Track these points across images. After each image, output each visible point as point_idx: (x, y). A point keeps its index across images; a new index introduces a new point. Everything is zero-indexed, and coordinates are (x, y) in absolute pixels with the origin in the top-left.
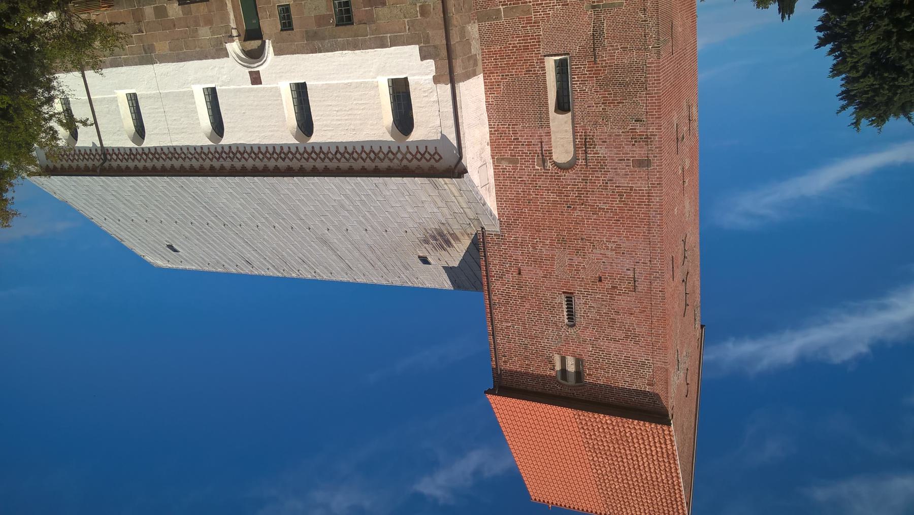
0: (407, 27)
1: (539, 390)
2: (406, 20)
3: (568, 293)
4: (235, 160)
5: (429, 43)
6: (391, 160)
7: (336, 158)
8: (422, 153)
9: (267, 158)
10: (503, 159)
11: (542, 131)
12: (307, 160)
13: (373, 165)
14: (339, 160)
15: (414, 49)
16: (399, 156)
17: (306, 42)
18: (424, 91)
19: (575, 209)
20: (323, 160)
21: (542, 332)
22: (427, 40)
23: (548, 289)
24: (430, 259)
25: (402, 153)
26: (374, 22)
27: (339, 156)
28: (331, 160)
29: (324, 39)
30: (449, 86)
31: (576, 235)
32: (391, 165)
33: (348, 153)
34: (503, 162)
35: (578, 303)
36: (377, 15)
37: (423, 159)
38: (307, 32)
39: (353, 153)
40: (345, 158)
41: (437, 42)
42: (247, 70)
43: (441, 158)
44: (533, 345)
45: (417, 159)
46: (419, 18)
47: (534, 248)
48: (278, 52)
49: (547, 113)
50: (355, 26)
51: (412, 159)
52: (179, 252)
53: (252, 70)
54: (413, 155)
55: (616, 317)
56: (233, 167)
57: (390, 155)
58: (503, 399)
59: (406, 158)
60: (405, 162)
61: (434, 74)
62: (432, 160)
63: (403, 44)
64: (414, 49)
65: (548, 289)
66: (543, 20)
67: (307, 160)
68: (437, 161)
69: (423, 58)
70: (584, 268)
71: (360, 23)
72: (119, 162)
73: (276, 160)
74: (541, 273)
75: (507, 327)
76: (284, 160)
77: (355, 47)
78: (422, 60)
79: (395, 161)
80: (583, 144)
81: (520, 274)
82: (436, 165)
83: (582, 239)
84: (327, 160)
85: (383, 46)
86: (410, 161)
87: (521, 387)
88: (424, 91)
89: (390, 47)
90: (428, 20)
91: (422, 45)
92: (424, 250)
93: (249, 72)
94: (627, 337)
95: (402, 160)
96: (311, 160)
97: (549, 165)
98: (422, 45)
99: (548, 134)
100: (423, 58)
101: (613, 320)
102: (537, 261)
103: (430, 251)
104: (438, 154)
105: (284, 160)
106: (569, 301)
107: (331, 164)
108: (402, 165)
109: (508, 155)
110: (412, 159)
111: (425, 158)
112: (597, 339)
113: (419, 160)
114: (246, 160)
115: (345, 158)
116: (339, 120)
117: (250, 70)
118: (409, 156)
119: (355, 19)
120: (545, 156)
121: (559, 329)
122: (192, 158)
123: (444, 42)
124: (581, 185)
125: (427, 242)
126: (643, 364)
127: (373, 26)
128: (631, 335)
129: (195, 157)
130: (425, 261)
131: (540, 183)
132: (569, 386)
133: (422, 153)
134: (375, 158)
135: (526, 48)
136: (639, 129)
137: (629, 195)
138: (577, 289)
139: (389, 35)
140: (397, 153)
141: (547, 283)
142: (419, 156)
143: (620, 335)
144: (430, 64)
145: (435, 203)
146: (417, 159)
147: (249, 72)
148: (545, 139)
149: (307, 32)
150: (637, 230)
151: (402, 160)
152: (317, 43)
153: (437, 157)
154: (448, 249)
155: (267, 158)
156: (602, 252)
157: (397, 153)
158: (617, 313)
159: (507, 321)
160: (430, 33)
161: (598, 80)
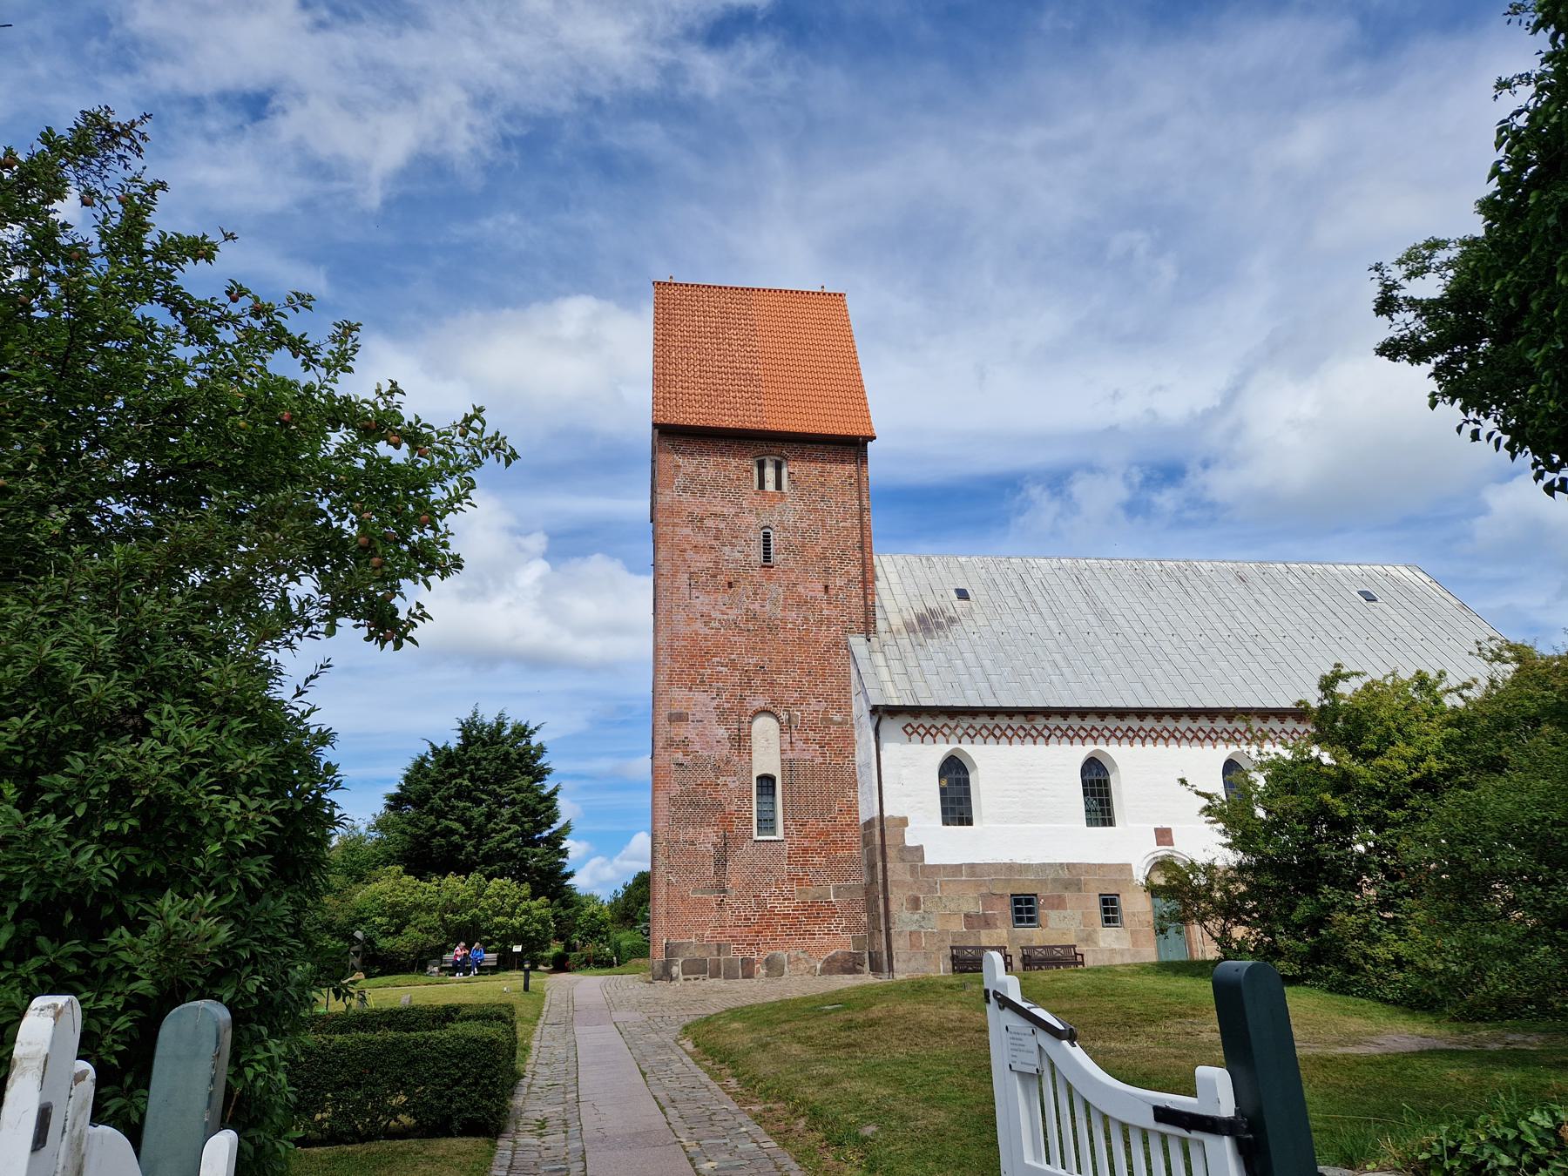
0: (938, 886)
1: (809, 446)
2: (939, 894)
3: (768, 567)
4: (1207, 730)
5: (911, 866)
6: (971, 726)
7: (1050, 730)
8: (928, 735)
9: (1156, 731)
10: (840, 724)
11: (790, 755)
12: (1094, 728)
13: (997, 720)
14: (1046, 727)
15: (930, 859)
16: (959, 732)
17: (1082, 878)
18: (920, 808)
19: (756, 665)
20: (1070, 728)
21: (801, 518)
22: (913, 870)
23: (792, 570)
24: (954, 596)
25: (956, 735)
26: (982, 896)
27: (1046, 733)
28: (1058, 728)
29: (1055, 880)
30: (886, 814)
31: (756, 635)
32: (971, 721)
33: (1032, 737)
34: (840, 720)
35: (757, 556)
36: (977, 903)
37: (927, 727)
38: (1079, 890)
39: (1062, 737)
40: (1037, 730)
41: (900, 865)
42: (1177, 847)
43: (904, 729)
44: (814, 502)
45: (936, 728)
46: (921, 896)
47: (806, 618)
48: (1125, 868)
49: (783, 776)
50: (1009, 892)
51: (942, 727)
52: (1361, 593)
53: (1167, 847)
54: (1222, 738)
55: (713, 542)
56: (1212, 720)
57: (972, 732)
58: (851, 432)
59: (950, 728)
60: (952, 724)
61: (906, 829)
62: (991, 728)
63: (945, 867)
64: (930, 859)
65: (792, 570)
66: (783, 881)
67: (1094, 728)
68: (910, 725)
69: (920, 849)
70: (748, 597)
71: (1001, 896)
72: (1194, 727)
73: (1141, 729)
74: (800, 589)
75: (845, 520)
76: (1130, 729)
77: (1010, 867)
78: (922, 846)
79: (965, 726)
80: (741, 741)
81: (826, 587)
82: (910, 720)
83: (748, 630)
84: (1064, 728)
85: (972, 866)
86: (945, 725)
87: (832, 447)
88: (920, 808)
89: (961, 865)
90: (910, 893)
91: (920, 864)
92: (958, 610)
93: (1173, 845)
94: (702, 520)
95: (957, 726)
96: (1088, 728)
97: (784, 717)
98: (920, 864)
99: (783, 752)
100: (920, 849)
101: (717, 538)
102: (802, 603)
103: (950, 606)
104: (907, 733)
105: (1130, 729)
106: (767, 557)
107: (1058, 723)
108: (956, 721)
109: (833, 728)
110: (942, 727)
111: (925, 728)
112: (736, 515)
113: (934, 726)
114: (1189, 729)
115: (1037, 730)
116: (1042, 778)
117: (1171, 848)
118: (946, 731)
119: (1008, 900)
120: (786, 727)
121: (781, 522)
122: (1055, 729)
123: (889, 866)
124: (747, 692)
125: (952, 620)
126: (684, 490)
127: (984, 890)
128: (697, 521)
129: (1275, 733)
130: (962, 594)
131: (796, 695)
132: (773, 455)
133: (928, 735)
134: (994, 729)
135: (805, 851)
136: (679, 756)
137: (693, 682)
138: (758, 573)
139: (964, 878)
140: (963, 735)
141: (793, 576)
142: (933, 731)
143: (709, 523)
144: (910, 841)
145: (922, 673)
146: (936, 728)
147: (1173, 845)
148: (787, 746)
149: (1079, 890)
150: (685, 643)
151: (957, 726)
152: (1065, 875)
153: (909, 730)
154: (925, 612)
155: (1156, 731)
156: (726, 617)
157: (963, 735)
158: (712, 547)
159: (845, 528)
160: (908, 878)
161: (723, 810)
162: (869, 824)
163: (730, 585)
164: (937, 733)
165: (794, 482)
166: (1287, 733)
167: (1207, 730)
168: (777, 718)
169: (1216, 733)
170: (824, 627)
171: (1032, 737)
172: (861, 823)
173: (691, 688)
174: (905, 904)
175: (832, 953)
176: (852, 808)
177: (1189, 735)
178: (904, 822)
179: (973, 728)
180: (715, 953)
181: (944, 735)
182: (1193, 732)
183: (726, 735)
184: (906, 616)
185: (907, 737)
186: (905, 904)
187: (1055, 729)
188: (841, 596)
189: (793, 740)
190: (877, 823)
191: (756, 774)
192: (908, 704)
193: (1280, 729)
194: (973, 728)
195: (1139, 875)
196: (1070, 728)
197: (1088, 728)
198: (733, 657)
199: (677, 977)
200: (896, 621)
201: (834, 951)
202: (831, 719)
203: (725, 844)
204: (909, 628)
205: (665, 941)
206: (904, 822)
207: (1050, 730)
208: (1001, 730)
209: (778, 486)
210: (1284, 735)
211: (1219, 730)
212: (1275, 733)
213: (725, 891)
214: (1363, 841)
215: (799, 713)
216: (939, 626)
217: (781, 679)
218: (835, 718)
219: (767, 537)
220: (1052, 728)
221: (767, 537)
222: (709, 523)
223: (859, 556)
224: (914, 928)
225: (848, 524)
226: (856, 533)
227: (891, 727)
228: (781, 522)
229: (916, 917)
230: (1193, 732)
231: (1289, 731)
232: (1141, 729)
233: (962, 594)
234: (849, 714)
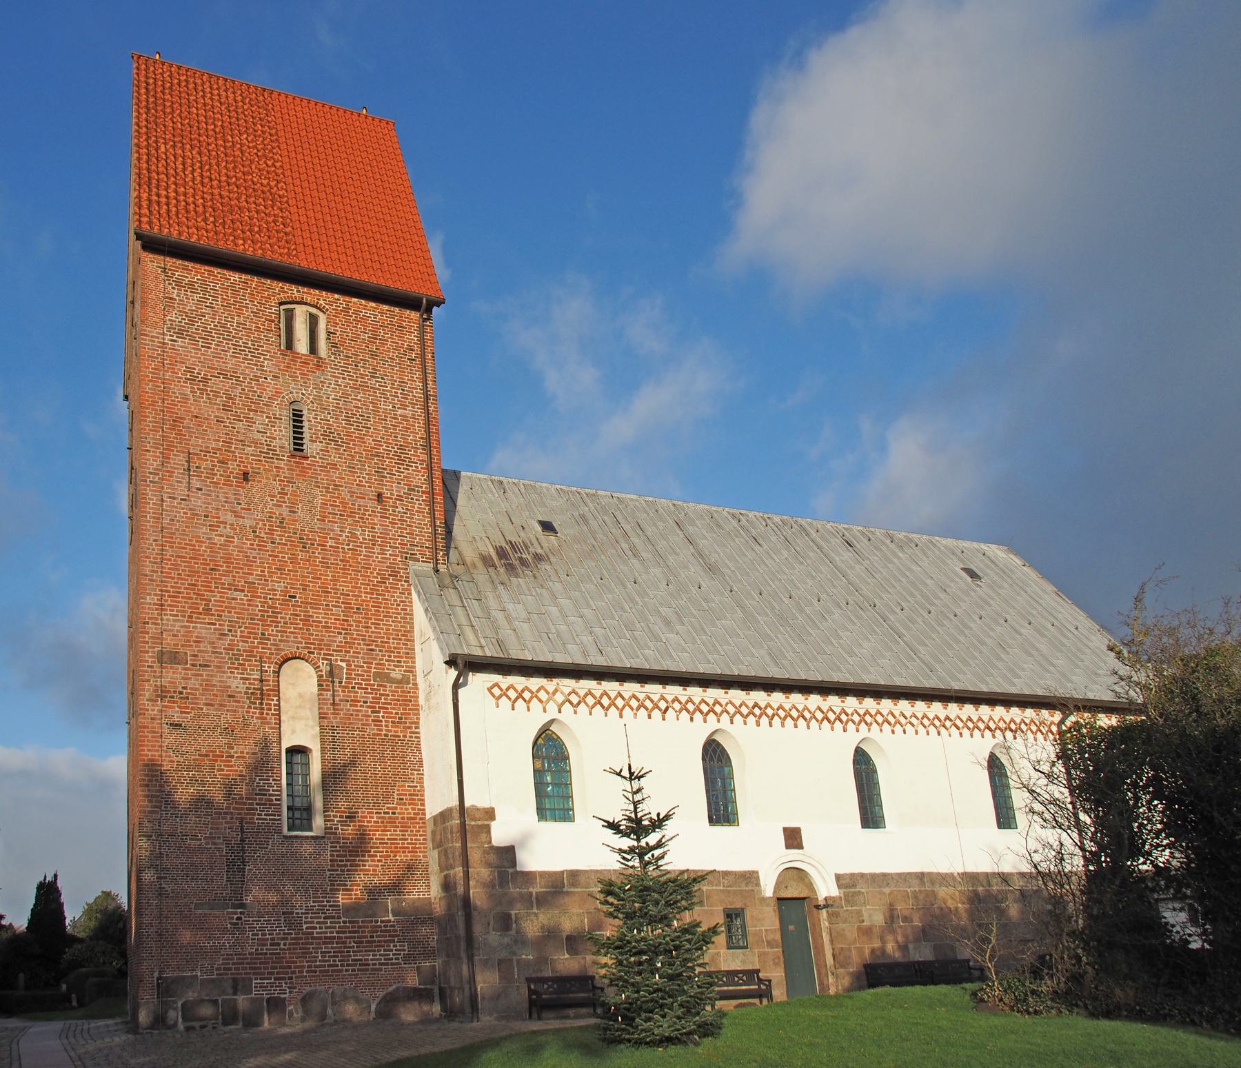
4: (838, 710)
7: (667, 701)
10: (399, 682)
12: (716, 702)
23: (334, 467)
24: (539, 528)
27: (663, 705)
30: (467, 804)
33: (646, 708)
35: (283, 435)
37: (504, 688)
40: (652, 701)
43: (489, 690)
45: (530, 691)
47: (354, 536)
48: (750, 878)
49: (323, 749)
52: (962, 569)
57: (575, 699)
73: (768, 705)
75: (404, 407)
89: (563, 872)
92: (545, 545)
95: (556, 691)
96: (711, 702)
97: (325, 668)
98: (511, 870)
99: (322, 717)
101: (227, 408)
104: (493, 696)
112: (256, 379)
114: (819, 708)
115: (652, 701)
121: (318, 399)
125: (538, 558)
126: (180, 334)
129: (906, 718)
130: (547, 527)
131: (340, 638)
134: (601, 696)
136: (175, 713)
137: (194, 608)
142: (527, 695)
143: (216, 384)
145: (508, 618)
151: (556, 691)
153: (496, 691)
154: (504, 545)
162: (443, 816)
163: (246, 476)
164: (531, 698)
165: (334, 345)
166: (918, 719)
167: (838, 710)
168: (316, 668)
169: (847, 714)
170: (377, 549)
171: (646, 708)
172: (428, 816)
173: (190, 617)
174: (492, 923)
175: (391, 989)
176: (416, 797)
177: (819, 715)
178: (490, 814)
179: (576, 694)
180: (230, 990)
181: (541, 701)
182: (823, 712)
183: (242, 688)
184: (483, 549)
185: (494, 701)
186: (492, 923)
187: (673, 701)
188: (400, 509)
189: (337, 702)
190: (456, 815)
191: (285, 745)
192: (496, 655)
193: (911, 714)
194: (576, 694)
195: (768, 888)
196: (690, 700)
197: (711, 702)
198: (251, 579)
199: (175, 1025)
200: (470, 555)
201: (394, 987)
202: (387, 676)
203: (242, 840)
204: (487, 561)
205: (156, 975)
206: (490, 814)
207: (667, 701)
208: (609, 698)
209: (313, 349)
210: (914, 720)
211: (849, 711)
212: (906, 718)
213: (242, 906)
214: (1105, 861)
215: (344, 664)
216: (523, 562)
217: (320, 615)
218: (393, 675)
219: (297, 417)
220: (670, 698)
221: (297, 417)
222: (216, 384)
223: (425, 457)
224: (504, 954)
225: (409, 413)
226: (419, 426)
227: (479, 682)
228: (318, 399)
229: (506, 940)
230: (823, 712)
231: (920, 716)
232: (768, 705)
233: (547, 527)
234: (411, 670)
